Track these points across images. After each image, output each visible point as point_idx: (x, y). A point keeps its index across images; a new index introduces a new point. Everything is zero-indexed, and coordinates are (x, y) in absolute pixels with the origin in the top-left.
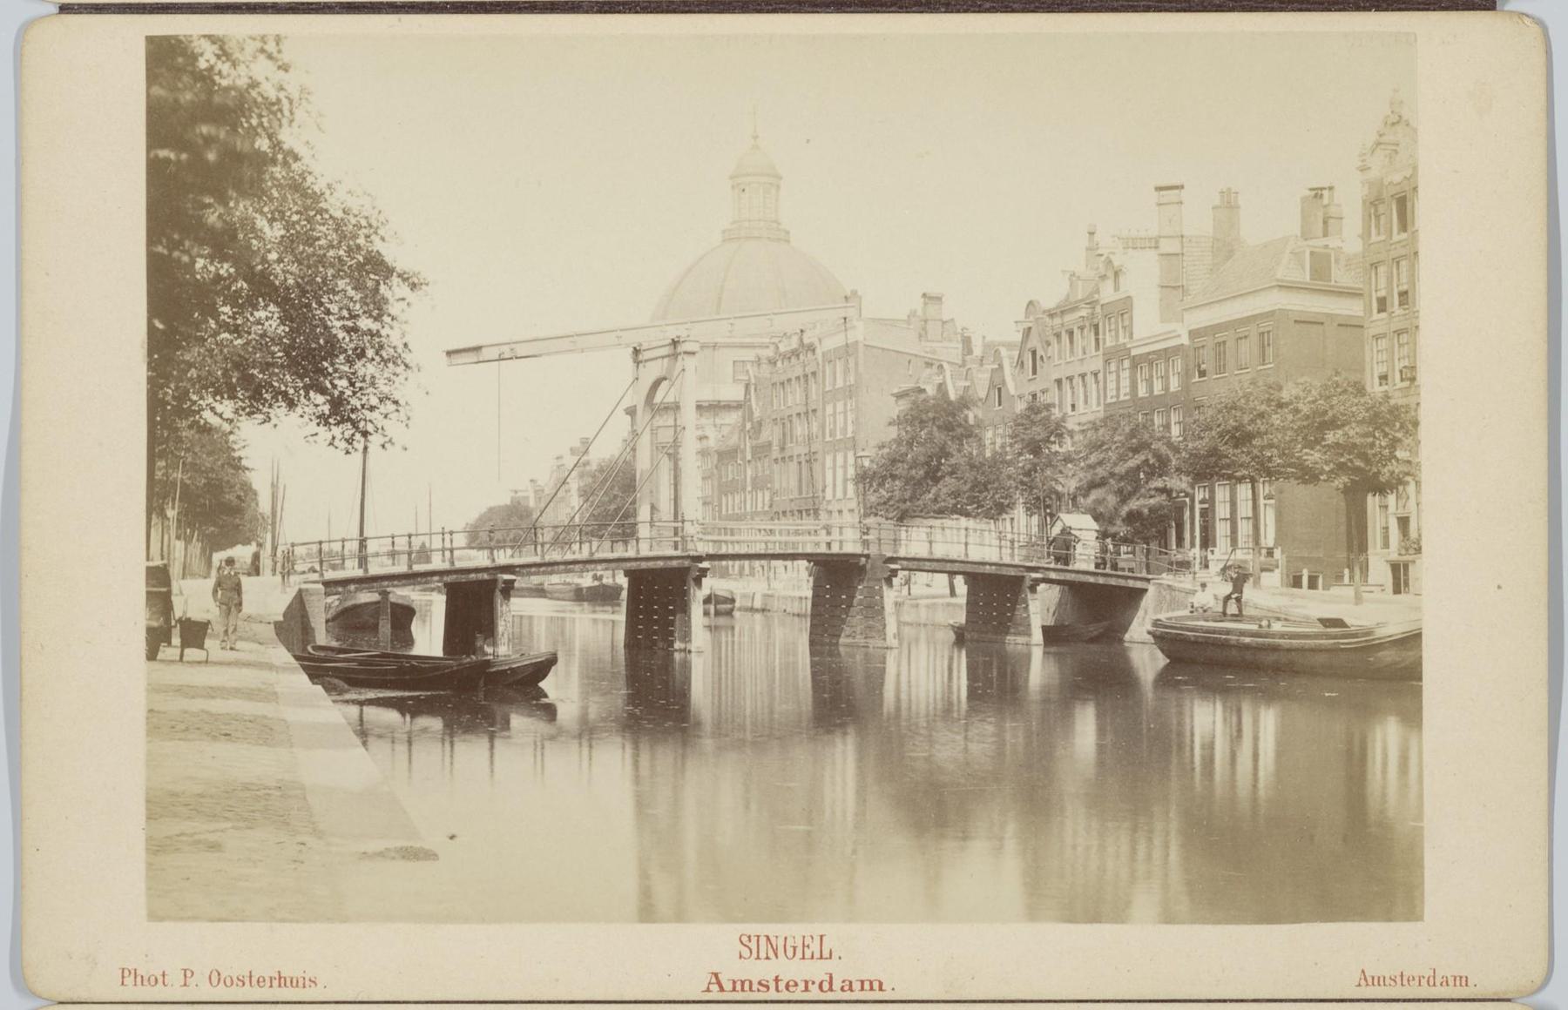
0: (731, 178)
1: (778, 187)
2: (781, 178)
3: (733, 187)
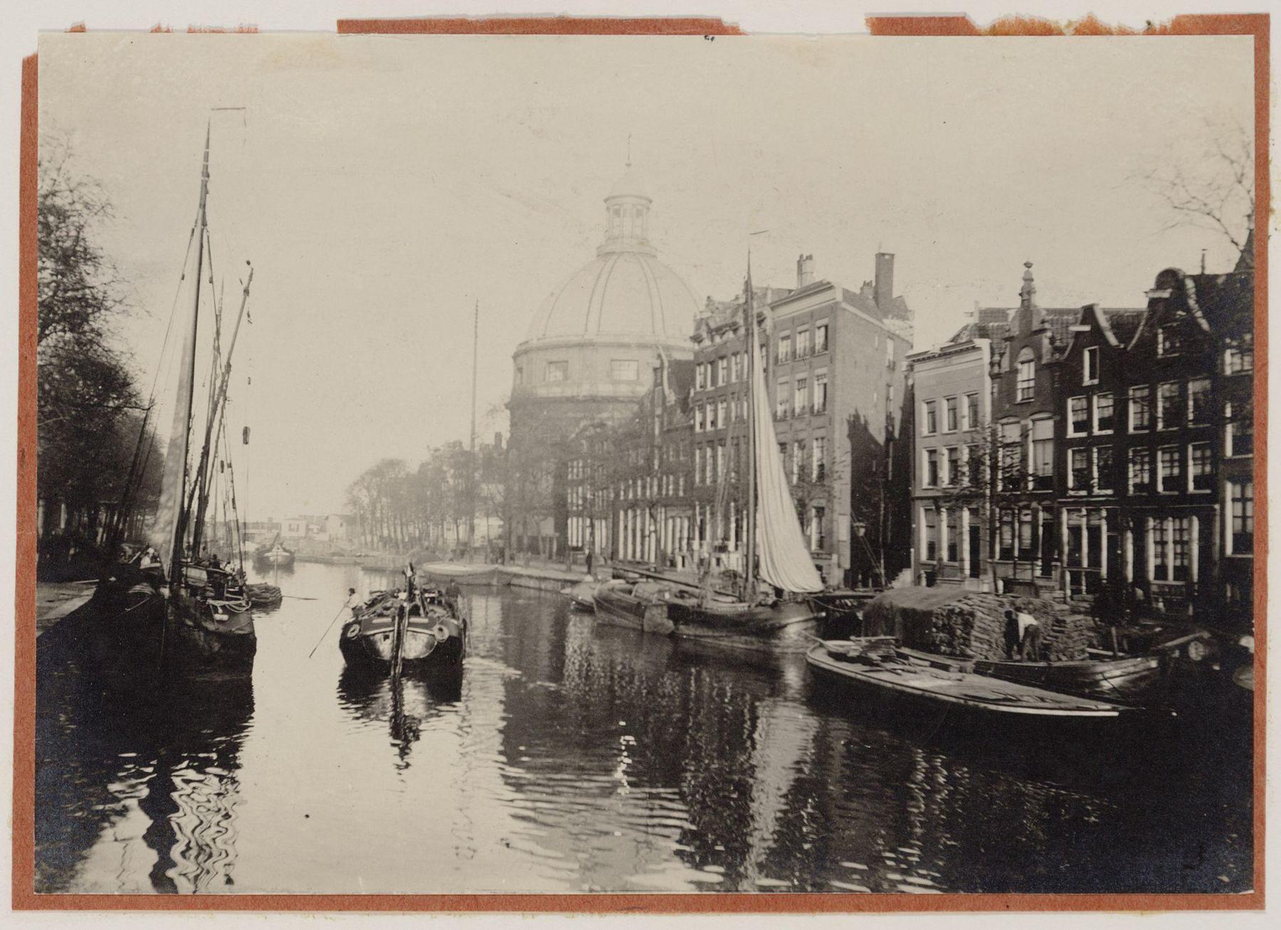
0: (606, 201)
2: (651, 202)
3: (608, 209)
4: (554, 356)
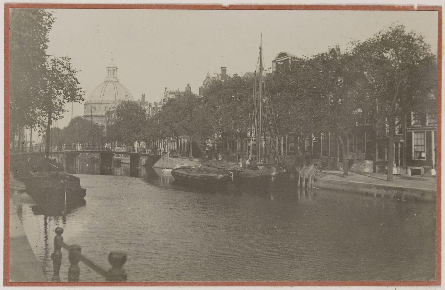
1: (117, 70)
4: (94, 105)
